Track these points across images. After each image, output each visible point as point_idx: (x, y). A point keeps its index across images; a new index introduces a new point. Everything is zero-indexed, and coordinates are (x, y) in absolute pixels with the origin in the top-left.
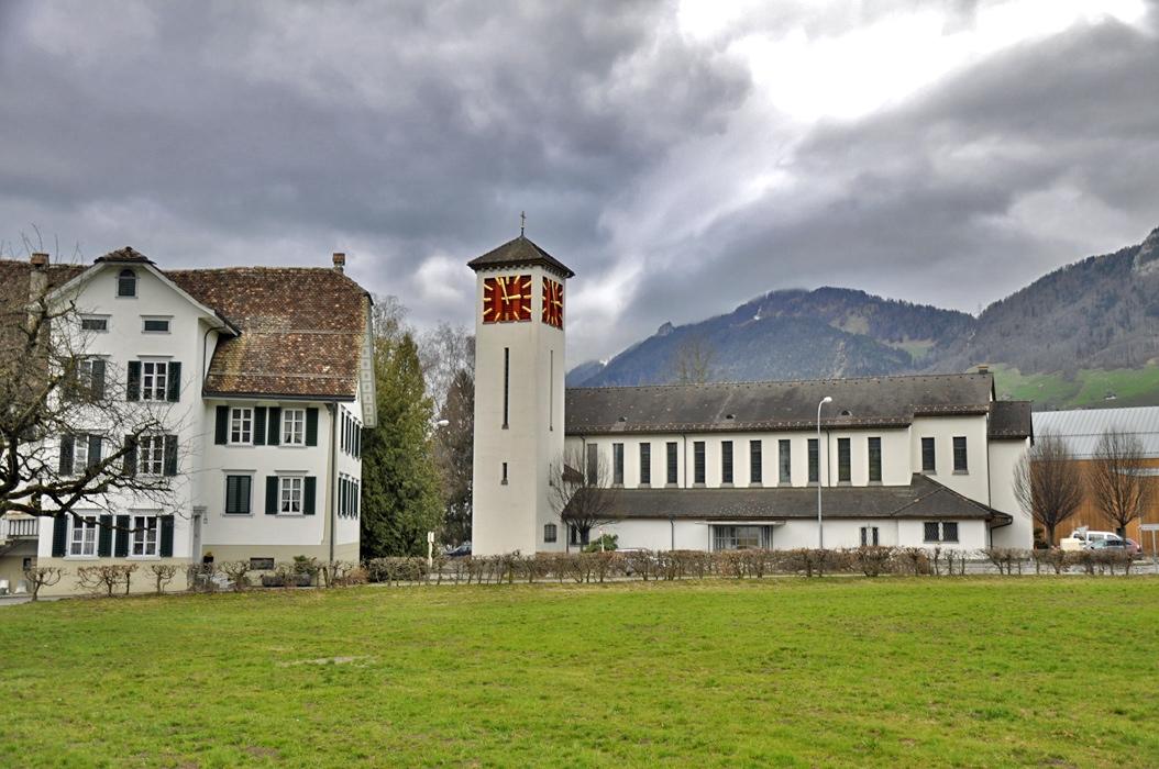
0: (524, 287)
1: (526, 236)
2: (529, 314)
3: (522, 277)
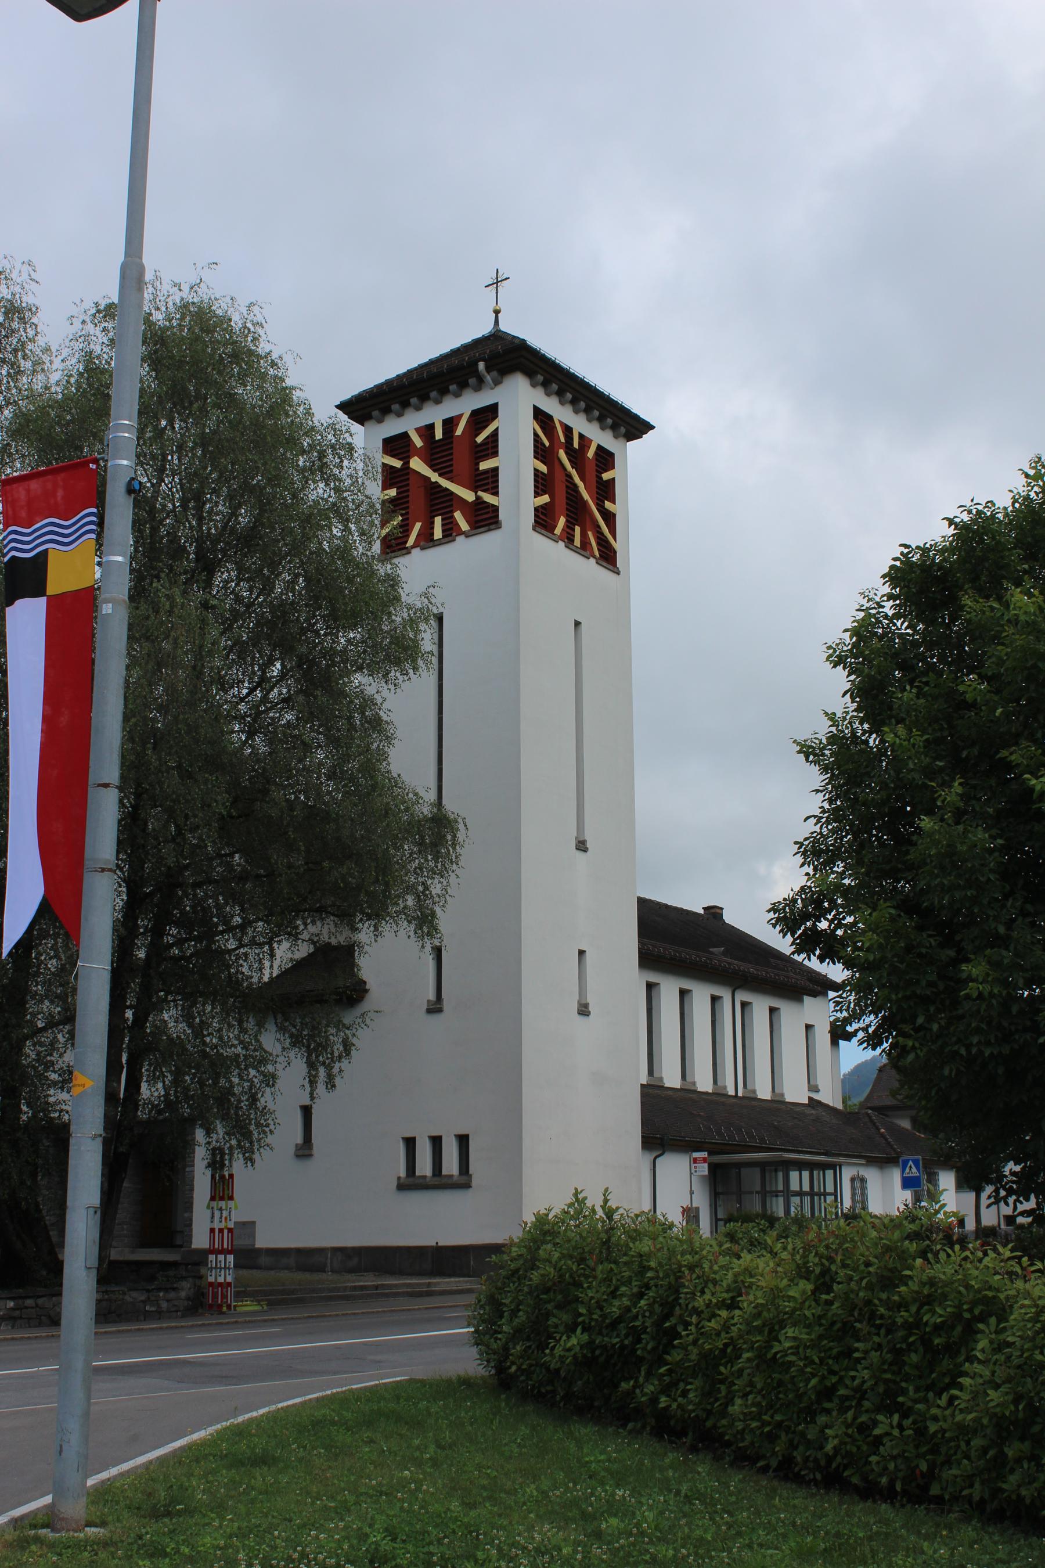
0: (480, 439)
1: (503, 327)
2: (495, 509)
3: (474, 413)
